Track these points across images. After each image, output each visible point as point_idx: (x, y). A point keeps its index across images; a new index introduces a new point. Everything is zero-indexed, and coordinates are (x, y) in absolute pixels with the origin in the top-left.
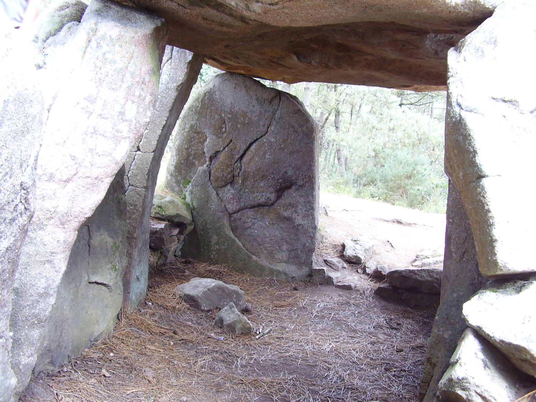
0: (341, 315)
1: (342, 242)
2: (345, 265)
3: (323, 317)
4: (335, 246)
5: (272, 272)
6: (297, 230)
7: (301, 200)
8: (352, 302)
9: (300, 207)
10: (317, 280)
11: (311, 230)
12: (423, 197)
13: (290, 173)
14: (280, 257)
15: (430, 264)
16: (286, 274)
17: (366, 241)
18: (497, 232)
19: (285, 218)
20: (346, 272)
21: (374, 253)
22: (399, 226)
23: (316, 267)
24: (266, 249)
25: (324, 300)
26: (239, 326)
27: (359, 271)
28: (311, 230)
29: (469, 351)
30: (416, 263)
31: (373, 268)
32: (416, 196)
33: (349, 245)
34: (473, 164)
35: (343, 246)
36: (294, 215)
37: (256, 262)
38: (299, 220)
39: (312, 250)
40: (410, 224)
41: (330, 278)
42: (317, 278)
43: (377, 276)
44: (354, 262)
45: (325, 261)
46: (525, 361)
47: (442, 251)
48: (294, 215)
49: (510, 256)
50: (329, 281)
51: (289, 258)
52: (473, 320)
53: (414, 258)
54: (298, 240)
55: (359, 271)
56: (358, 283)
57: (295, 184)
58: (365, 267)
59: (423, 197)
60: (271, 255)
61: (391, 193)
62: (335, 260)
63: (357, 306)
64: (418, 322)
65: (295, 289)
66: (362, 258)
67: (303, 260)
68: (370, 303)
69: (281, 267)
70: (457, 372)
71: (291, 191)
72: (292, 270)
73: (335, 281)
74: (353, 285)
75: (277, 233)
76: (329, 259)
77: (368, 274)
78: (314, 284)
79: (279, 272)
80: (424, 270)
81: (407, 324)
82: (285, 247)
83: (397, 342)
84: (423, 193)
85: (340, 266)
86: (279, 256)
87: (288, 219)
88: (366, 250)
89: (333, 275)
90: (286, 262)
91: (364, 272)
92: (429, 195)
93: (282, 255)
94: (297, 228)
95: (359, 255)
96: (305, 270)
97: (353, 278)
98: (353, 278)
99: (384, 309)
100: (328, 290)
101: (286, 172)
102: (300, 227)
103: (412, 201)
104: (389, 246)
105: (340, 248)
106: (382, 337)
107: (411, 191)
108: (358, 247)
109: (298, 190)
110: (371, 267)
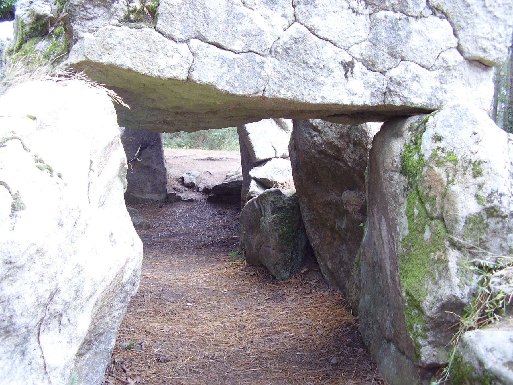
0: (192, 213)
1: (181, 176)
2: (186, 189)
3: (183, 216)
4: (177, 180)
5: (144, 200)
6: (155, 172)
7: (154, 154)
8: (195, 207)
9: (154, 158)
10: (172, 199)
11: (163, 171)
12: (220, 140)
13: (145, 139)
14: (147, 190)
15: (235, 179)
16: (152, 200)
17: (195, 173)
18: (255, 149)
19: (146, 167)
20: (188, 192)
21: (201, 179)
22: (212, 162)
23: (169, 192)
24: (137, 187)
25: (180, 209)
26: (144, 224)
27: (195, 190)
28: (163, 171)
29: (253, 183)
30: (227, 180)
31: (203, 187)
32: (214, 140)
33: (185, 176)
34: (246, 131)
35: (182, 178)
36: (151, 164)
37: (133, 196)
38: (155, 166)
39: (166, 183)
40: (218, 160)
41: (180, 197)
42: (172, 199)
43: (206, 191)
44: (191, 186)
45: (174, 188)
46: (268, 182)
47: (241, 170)
48: (151, 164)
49: (260, 155)
50: (179, 199)
51: (152, 190)
52: (252, 175)
53: (225, 178)
54: (156, 178)
55: (195, 190)
56: (196, 197)
57: (149, 145)
58: (198, 188)
59: (220, 140)
60: (141, 190)
61: (194, 141)
62: (180, 187)
63: (199, 208)
64: (234, 210)
65: (160, 207)
66: (195, 183)
67: (161, 189)
68: (206, 206)
69: (149, 196)
70: (251, 190)
71: (147, 150)
72: (156, 197)
73: (183, 198)
74: (194, 199)
75: (142, 176)
76: (176, 186)
77: (201, 192)
78: (171, 203)
79: (148, 200)
80: (233, 182)
81: (228, 211)
82: (148, 184)
83: (225, 219)
84: (220, 137)
85: (183, 189)
86: (146, 190)
87: (148, 167)
88: (197, 178)
89: (181, 195)
90: (151, 193)
91: (198, 191)
92: (224, 138)
93: (149, 189)
94: (154, 172)
95: (193, 181)
96: (163, 196)
97: (193, 195)
98: (193, 195)
99: (215, 207)
100: (180, 204)
101: (143, 139)
102: (156, 171)
103: (212, 145)
104: (209, 174)
105: (180, 180)
106: (217, 219)
107: (210, 137)
108: (191, 177)
109: (151, 148)
110: (201, 186)
